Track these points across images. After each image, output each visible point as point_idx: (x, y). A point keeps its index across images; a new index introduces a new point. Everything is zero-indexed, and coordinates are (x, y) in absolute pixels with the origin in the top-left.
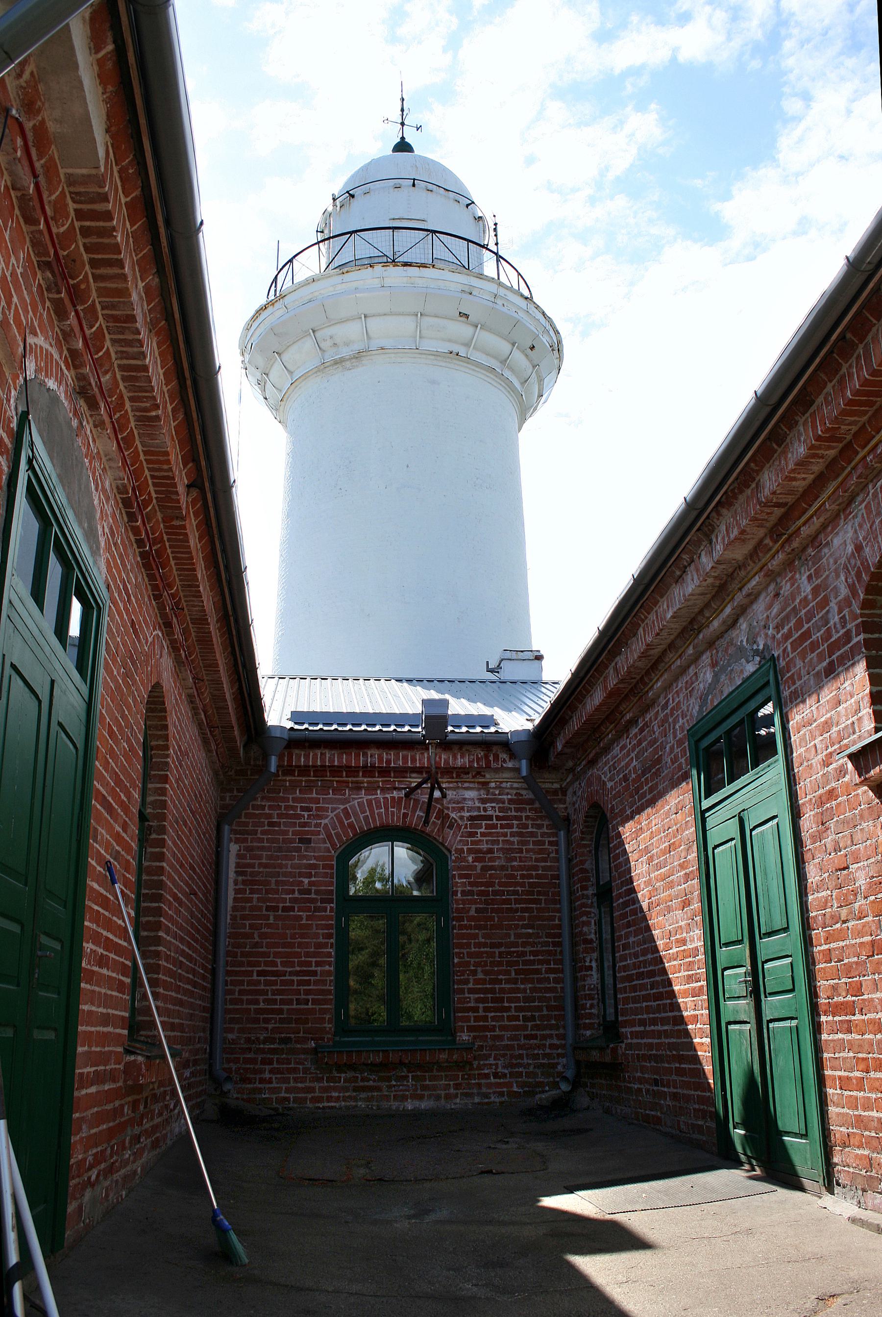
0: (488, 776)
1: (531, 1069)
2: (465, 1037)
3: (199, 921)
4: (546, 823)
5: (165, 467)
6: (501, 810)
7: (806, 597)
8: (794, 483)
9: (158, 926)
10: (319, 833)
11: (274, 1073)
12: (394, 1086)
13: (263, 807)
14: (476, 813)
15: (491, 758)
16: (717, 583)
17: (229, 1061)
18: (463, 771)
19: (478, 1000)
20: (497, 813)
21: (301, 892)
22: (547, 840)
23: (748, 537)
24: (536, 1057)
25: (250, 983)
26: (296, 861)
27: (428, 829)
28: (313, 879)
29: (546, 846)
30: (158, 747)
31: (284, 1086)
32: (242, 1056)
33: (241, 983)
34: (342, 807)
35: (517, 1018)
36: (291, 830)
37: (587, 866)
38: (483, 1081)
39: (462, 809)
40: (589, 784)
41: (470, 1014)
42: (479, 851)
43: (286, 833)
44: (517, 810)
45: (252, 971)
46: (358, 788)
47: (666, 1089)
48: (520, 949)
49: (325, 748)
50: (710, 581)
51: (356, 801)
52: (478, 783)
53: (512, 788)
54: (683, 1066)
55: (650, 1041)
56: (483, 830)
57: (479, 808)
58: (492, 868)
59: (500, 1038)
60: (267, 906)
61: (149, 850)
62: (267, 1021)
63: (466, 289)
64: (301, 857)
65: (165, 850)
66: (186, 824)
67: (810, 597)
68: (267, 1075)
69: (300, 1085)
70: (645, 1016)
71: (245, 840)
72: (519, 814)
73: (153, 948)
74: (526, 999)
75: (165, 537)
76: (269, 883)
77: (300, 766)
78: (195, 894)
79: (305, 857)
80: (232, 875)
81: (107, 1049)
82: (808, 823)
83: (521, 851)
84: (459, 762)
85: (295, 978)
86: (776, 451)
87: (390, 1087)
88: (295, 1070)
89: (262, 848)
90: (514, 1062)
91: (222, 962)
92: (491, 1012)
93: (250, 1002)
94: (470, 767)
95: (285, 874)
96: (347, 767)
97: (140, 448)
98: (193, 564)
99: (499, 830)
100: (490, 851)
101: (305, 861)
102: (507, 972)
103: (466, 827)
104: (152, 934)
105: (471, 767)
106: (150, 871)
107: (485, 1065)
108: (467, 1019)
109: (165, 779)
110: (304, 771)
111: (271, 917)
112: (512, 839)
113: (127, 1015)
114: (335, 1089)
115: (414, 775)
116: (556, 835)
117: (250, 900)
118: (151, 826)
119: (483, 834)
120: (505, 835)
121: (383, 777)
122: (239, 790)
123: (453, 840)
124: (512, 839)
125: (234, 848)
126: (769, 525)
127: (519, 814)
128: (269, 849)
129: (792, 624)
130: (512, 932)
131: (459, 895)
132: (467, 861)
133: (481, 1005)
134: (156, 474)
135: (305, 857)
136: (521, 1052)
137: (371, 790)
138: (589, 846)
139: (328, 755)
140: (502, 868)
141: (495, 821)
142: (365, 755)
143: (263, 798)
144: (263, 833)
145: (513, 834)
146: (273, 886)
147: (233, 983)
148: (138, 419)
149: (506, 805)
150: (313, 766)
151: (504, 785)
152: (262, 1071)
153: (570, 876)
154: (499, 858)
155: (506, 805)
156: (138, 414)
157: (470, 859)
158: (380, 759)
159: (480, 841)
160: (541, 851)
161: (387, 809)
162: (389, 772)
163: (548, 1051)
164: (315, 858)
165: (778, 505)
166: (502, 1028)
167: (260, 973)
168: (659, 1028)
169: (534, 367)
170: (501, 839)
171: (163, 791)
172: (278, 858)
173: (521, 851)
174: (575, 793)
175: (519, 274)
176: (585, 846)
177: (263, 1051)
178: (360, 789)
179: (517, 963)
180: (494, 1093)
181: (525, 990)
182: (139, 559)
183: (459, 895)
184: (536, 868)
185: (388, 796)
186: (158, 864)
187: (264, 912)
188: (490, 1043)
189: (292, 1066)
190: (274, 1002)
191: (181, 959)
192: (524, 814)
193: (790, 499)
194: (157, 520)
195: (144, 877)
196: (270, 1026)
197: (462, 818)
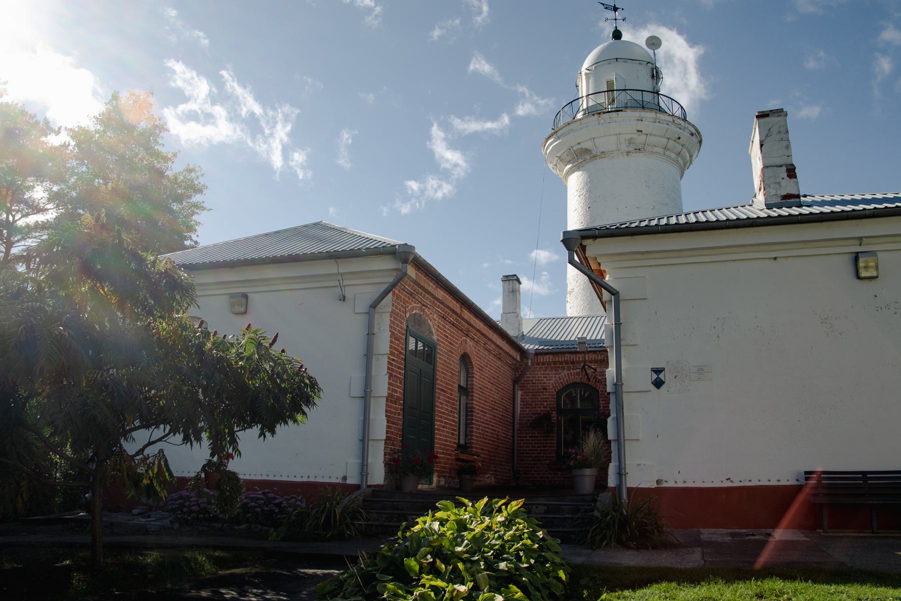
46: (563, 368)
110: (543, 364)
125: (520, 393)
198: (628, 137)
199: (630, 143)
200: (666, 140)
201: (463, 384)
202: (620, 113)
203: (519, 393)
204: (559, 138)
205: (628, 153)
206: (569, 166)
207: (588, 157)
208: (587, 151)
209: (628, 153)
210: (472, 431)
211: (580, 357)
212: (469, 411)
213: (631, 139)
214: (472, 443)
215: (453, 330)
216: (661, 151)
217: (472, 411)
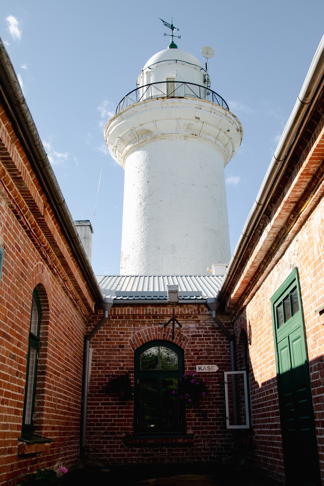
0: (199, 318)
1: (220, 446)
2: (190, 432)
3: (72, 382)
4: (225, 338)
5: (30, 197)
6: (205, 332)
7: (306, 242)
8: (296, 193)
9: (44, 385)
10: (127, 343)
11: (108, 448)
12: (159, 454)
13: (104, 332)
14: (195, 334)
15: (200, 310)
16: (275, 236)
17: (89, 442)
18: (188, 316)
19: (196, 416)
20: (204, 334)
21: (120, 368)
22: (225, 345)
23: (283, 216)
24: (222, 441)
25: (98, 408)
26: (118, 355)
27: (174, 341)
28: (125, 363)
29: (225, 348)
30: (45, 310)
31: (112, 453)
32: (94, 440)
33: (94, 408)
34: (137, 332)
35: (213, 424)
36: (116, 342)
37: (242, 356)
38: (198, 452)
39: (189, 332)
40: (241, 321)
41: (193, 422)
42: (196, 350)
43: (113, 343)
44: (212, 332)
45: (99, 403)
46: (143, 323)
47: (269, 458)
48: (214, 393)
49: (129, 306)
50: (272, 235)
51: (143, 330)
52: (195, 321)
53: (210, 323)
54: (274, 447)
55: (263, 435)
56: (197, 341)
57: (196, 331)
58: (202, 357)
59: (206, 432)
60: (105, 375)
61: (41, 353)
62: (105, 425)
63: (198, 106)
64: (120, 354)
65: (47, 353)
66: (62, 341)
67: (308, 242)
68: (105, 449)
69: (119, 453)
70: (261, 424)
71: (96, 347)
72: (213, 334)
73: (41, 395)
74: (217, 415)
75: (37, 224)
76: (106, 365)
77: (119, 315)
78: (69, 370)
79: (122, 353)
80: (90, 362)
81: (6, 439)
82: (309, 341)
83: (214, 350)
84: (187, 312)
85: (117, 406)
86: (288, 179)
87: (158, 454)
88: (117, 446)
89: (103, 350)
90: (212, 443)
91: (86, 398)
92: (201, 421)
93: (97, 416)
94: (191, 314)
95: (113, 361)
96: (139, 315)
97: (17, 190)
98: (52, 234)
99: (204, 341)
100: (201, 350)
101: (121, 355)
102: (209, 403)
103: (190, 340)
104: (41, 389)
105: (191, 314)
106: (41, 362)
107: (199, 445)
108: (191, 424)
109: (48, 323)
110: (121, 317)
111: (107, 380)
112: (210, 345)
113: (21, 424)
114: (134, 455)
115: (167, 318)
116: (229, 343)
117: (98, 372)
118: (42, 343)
119: (198, 343)
120: (207, 343)
121: (154, 318)
122: (94, 325)
123: (186, 346)
124: (210, 345)
125: (91, 350)
126: (290, 211)
127: (213, 334)
128: (106, 350)
129: (302, 253)
130: (211, 386)
131: (188, 369)
132: (191, 355)
133: (197, 418)
134: (27, 199)
135: (122, 353)
136: (215, 439)
137: (150, 324)
138: (243, 348)
139: (130, 310)
140: (206, 357)
141: (203, 337)
142: (146, 309)
143: (104, 329)
144: (104, 343)
145: (210, 343)
146: (108, 366)
147: (91, 408)
148: (13, 178)
149: (208, 330)
150: (125, 315)
151: (206, 321)
152: (102, 447)
153: (235, 360)
154: (205, 353)
155: (208, 330)
156: (13, 176)
157: (192, 354)
158: (153, 310)
159: (196, 346)
160: (223, 350)
161: (156, 332)
162: (157, 317)
163: (227, 438)
164: (126, 354)
165: (292, 202)
166: (207, 428)
167: (102, 404)
168: (265, 429)
169: (230, 139)
170: (205, 345)
171: (47, 328)
172: (110, 354)
173: (214, 350)
174: (237, 324)
175: (223, 99)
176: (241, 348)
177: (103, 438)
178: (144, 324)
179: (213, 399)
180: (203, 457)
181: (217, 411)
182: (25, 233)
183: (188, 369)
184: (221, 357)
185: (157, 327)
186: (44, 359)
187: (104, 377)
188: (201, 435)
189: (116, 444)
190: (108, 416)
191: (59, 398)
192: (215, 334)
193: (296, 200)
194: (32, 218)
195: (39, 365)
196: (106, 427)
197: (188, 336)
199: (187, 128)
200: (218, 131)
201: (34, 331)
203: (91, 351)
204: (123, 119)
205: (186, 136)
206: (128, 147)
207: (149, 138)
209: (186, 136)
210: (43, 403)
211: (169, 310)
212: (40, 371)
213: (189, 124)
214: (42, 422)
215: (28, 242)
216: (213, 139)
217: (44, 373)
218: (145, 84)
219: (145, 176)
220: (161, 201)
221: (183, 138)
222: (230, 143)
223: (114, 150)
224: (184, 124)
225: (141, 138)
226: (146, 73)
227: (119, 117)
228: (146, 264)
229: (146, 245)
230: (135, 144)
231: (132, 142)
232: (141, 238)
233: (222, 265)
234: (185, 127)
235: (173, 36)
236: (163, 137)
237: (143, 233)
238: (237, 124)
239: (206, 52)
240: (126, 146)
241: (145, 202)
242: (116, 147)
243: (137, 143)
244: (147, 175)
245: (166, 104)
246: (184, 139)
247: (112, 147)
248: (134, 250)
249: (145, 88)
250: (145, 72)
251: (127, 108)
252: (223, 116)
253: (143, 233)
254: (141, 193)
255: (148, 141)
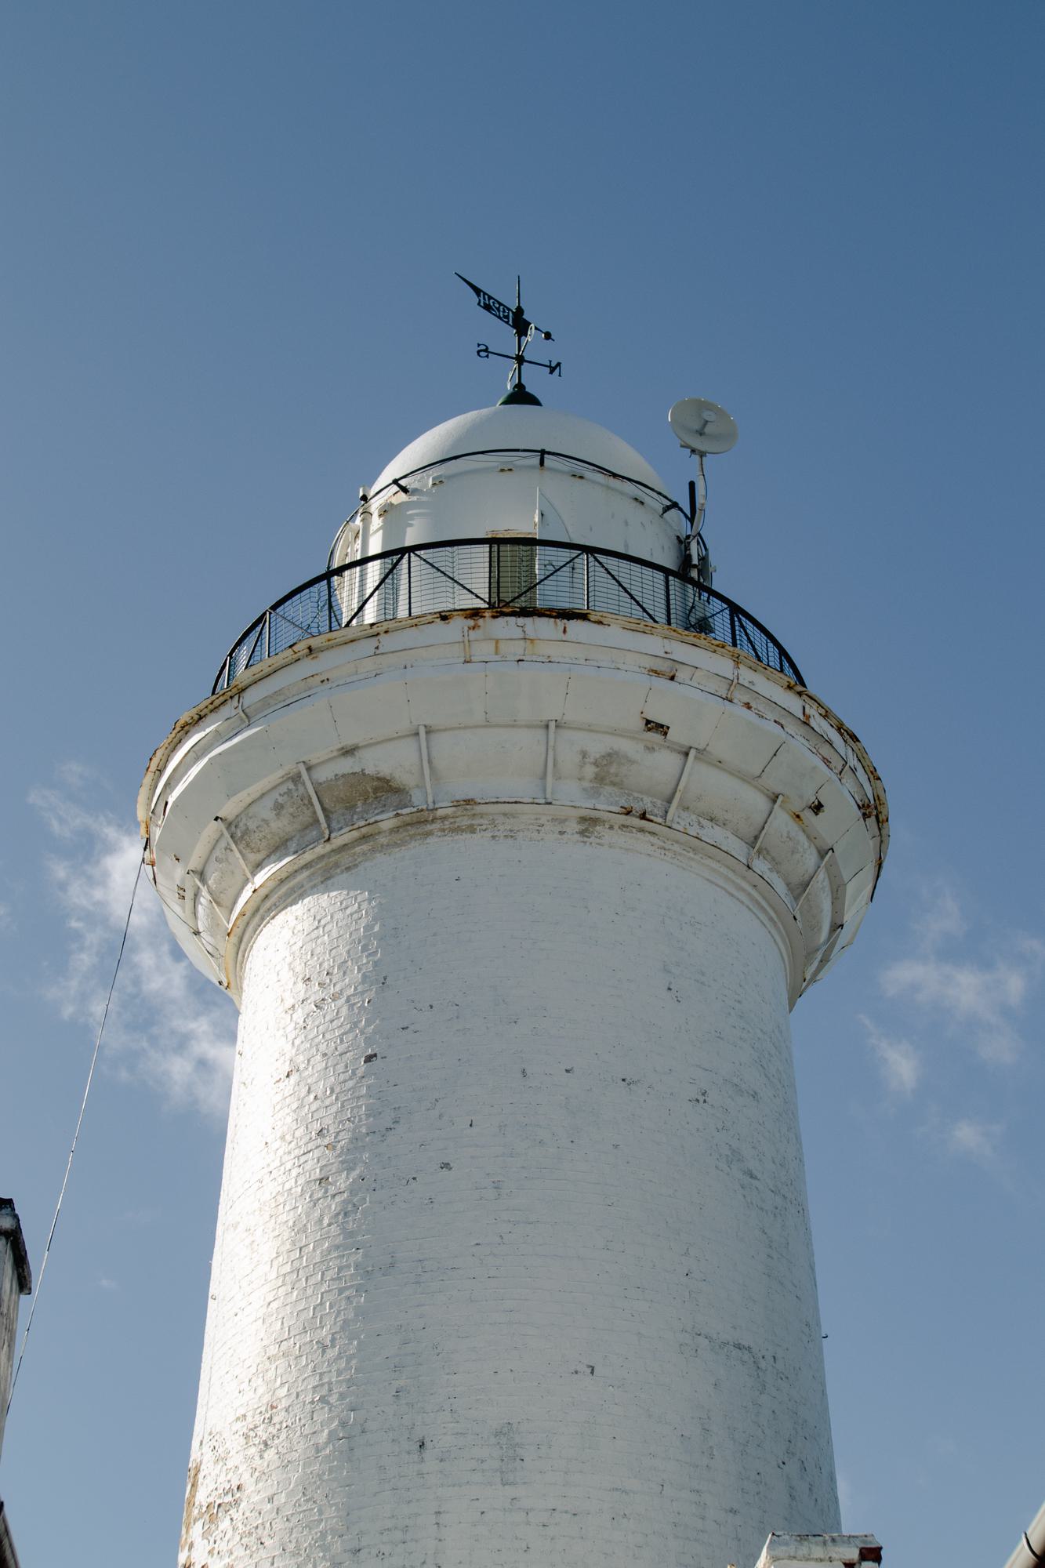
63: (663, 666)
169: (822, 854)
175: (783, 653)
198: (597, 746)
199: (600, 779)
200: (762, 803)
202: (574, 626)
204: (248, 719)
205: (589, 823)
207: (387, 821)
208: (385, 790)
209: (589, 823)
213: (611, 756)
218: (375, 548)
219: (355, 1025)
220: (446, 1166)
221: (573, 826)
222: (822, 875)
223: (189, 895)
224: (584, 755)
225: (341, 821)
226: (385, 512)
227: (227, 710)
228: (338, 1546)
229: (343, 1424)
230: (308, 856)
231: (293, 846)
232: (314, 1381)
233: (818, 1552)
234: (590, 771)
235: (520, 360)
236: (465, 822)
237: (331, 1353)
238: (861, 774)
239: (697, 426)
240: (258, 866)
241: (350, 1170)
242: (202, 875)
243: (321, 849)
244: (368, 1023)
245: (492, 646)
246: (582, 833)
247: (179, 872)
248: (270, 1454)
249: (374, 570)
250: (375, 505)
251: (278, 661)
252: (792, 728)
253: (331, 1353)
254: (328, 1121)
255: (382, 840)
